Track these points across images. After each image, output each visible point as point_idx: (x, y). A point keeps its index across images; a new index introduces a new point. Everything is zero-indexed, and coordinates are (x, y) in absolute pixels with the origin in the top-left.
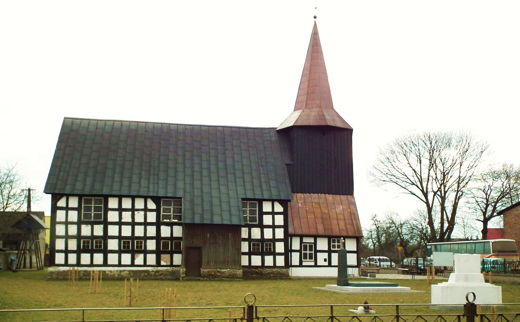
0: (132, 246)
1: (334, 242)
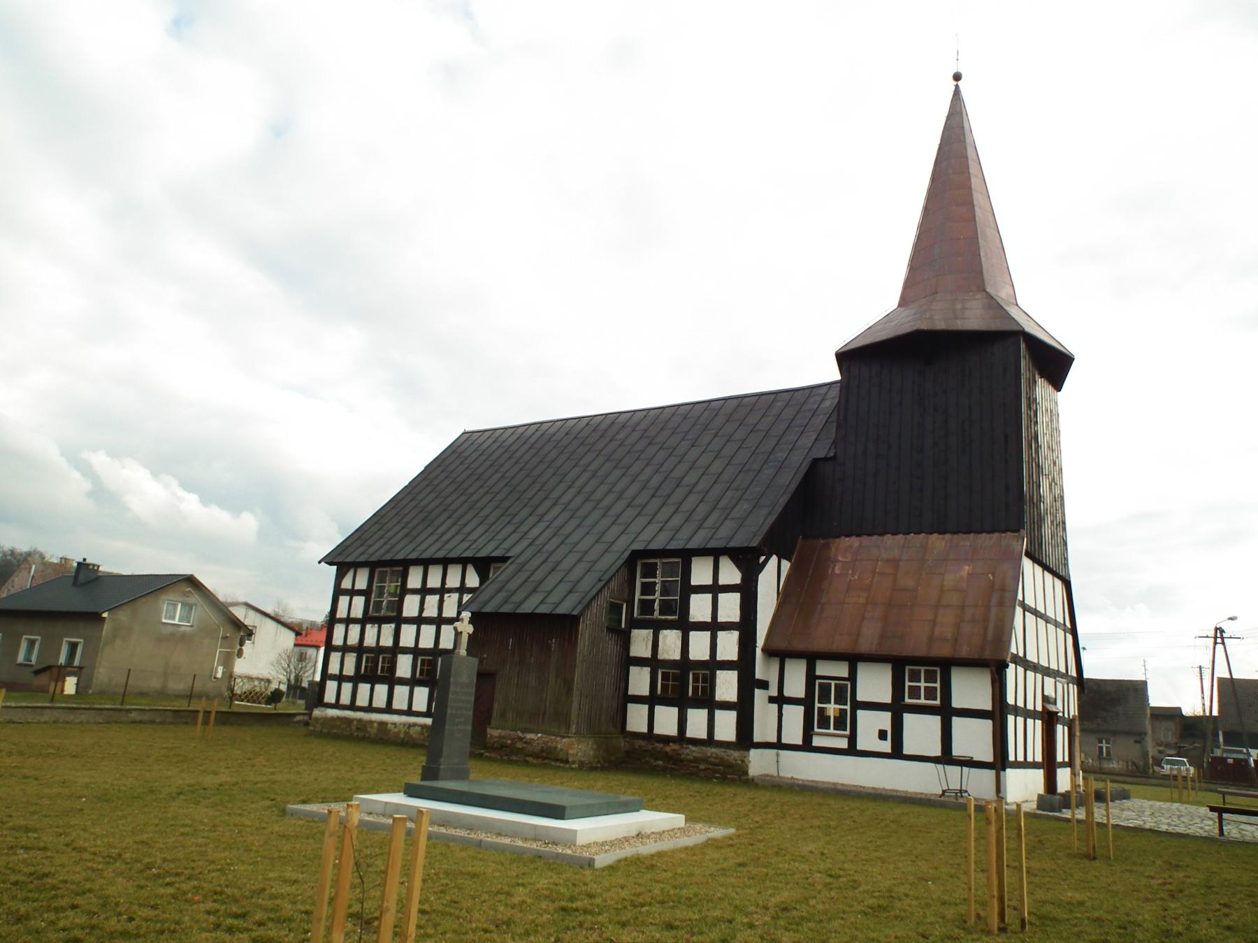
1: (915, 677)
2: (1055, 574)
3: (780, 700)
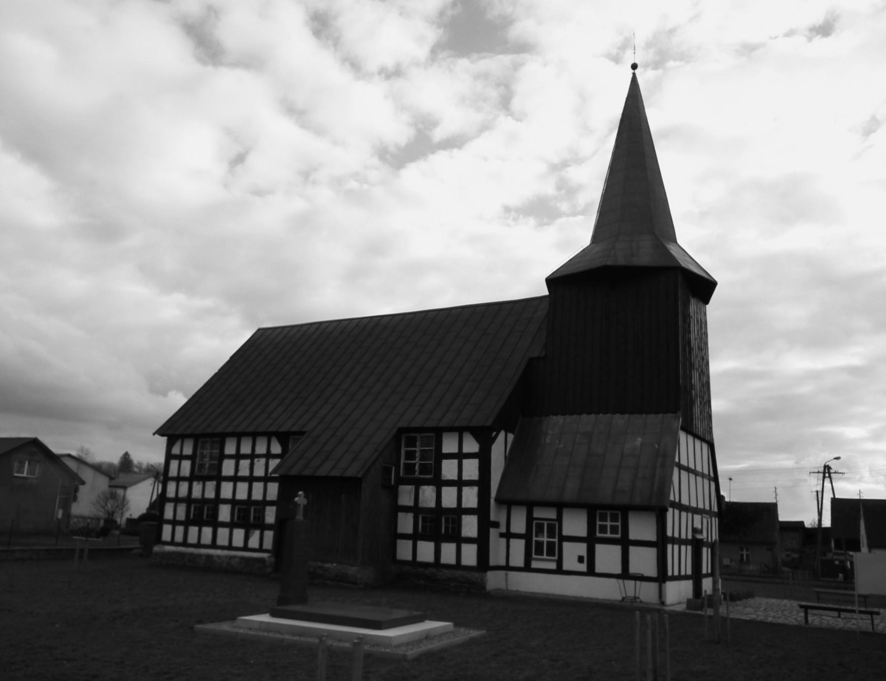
0: (247, 515)
1: (603, 518)
2: (702, 440)
3: (508, 535)
